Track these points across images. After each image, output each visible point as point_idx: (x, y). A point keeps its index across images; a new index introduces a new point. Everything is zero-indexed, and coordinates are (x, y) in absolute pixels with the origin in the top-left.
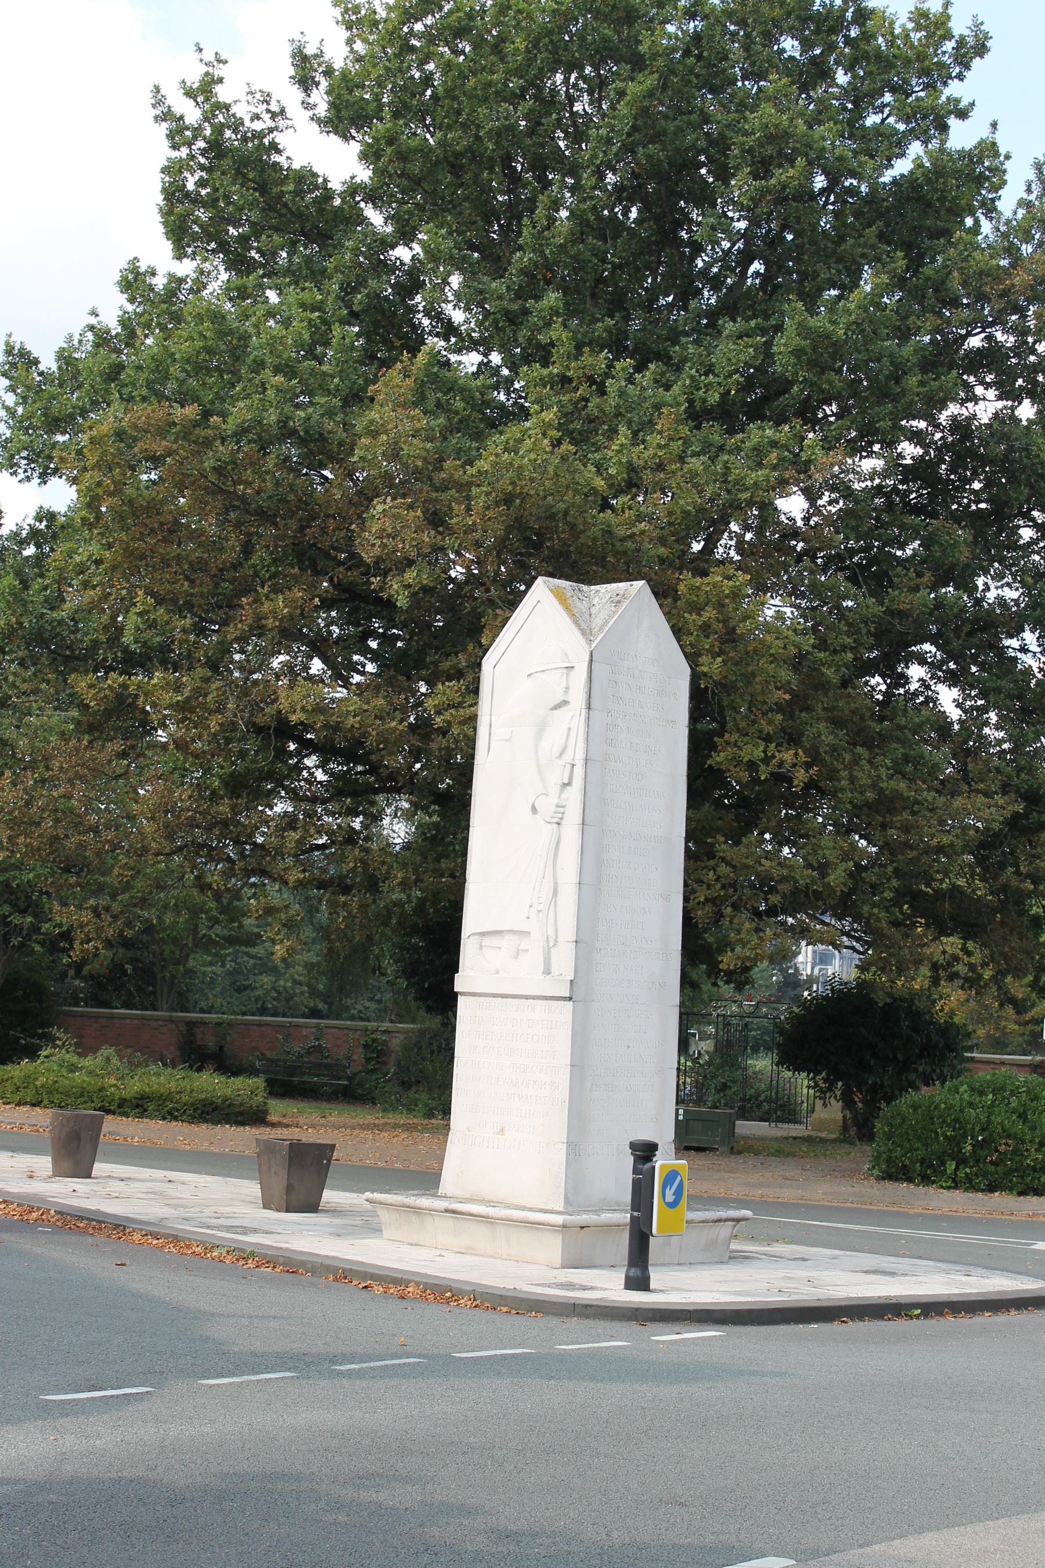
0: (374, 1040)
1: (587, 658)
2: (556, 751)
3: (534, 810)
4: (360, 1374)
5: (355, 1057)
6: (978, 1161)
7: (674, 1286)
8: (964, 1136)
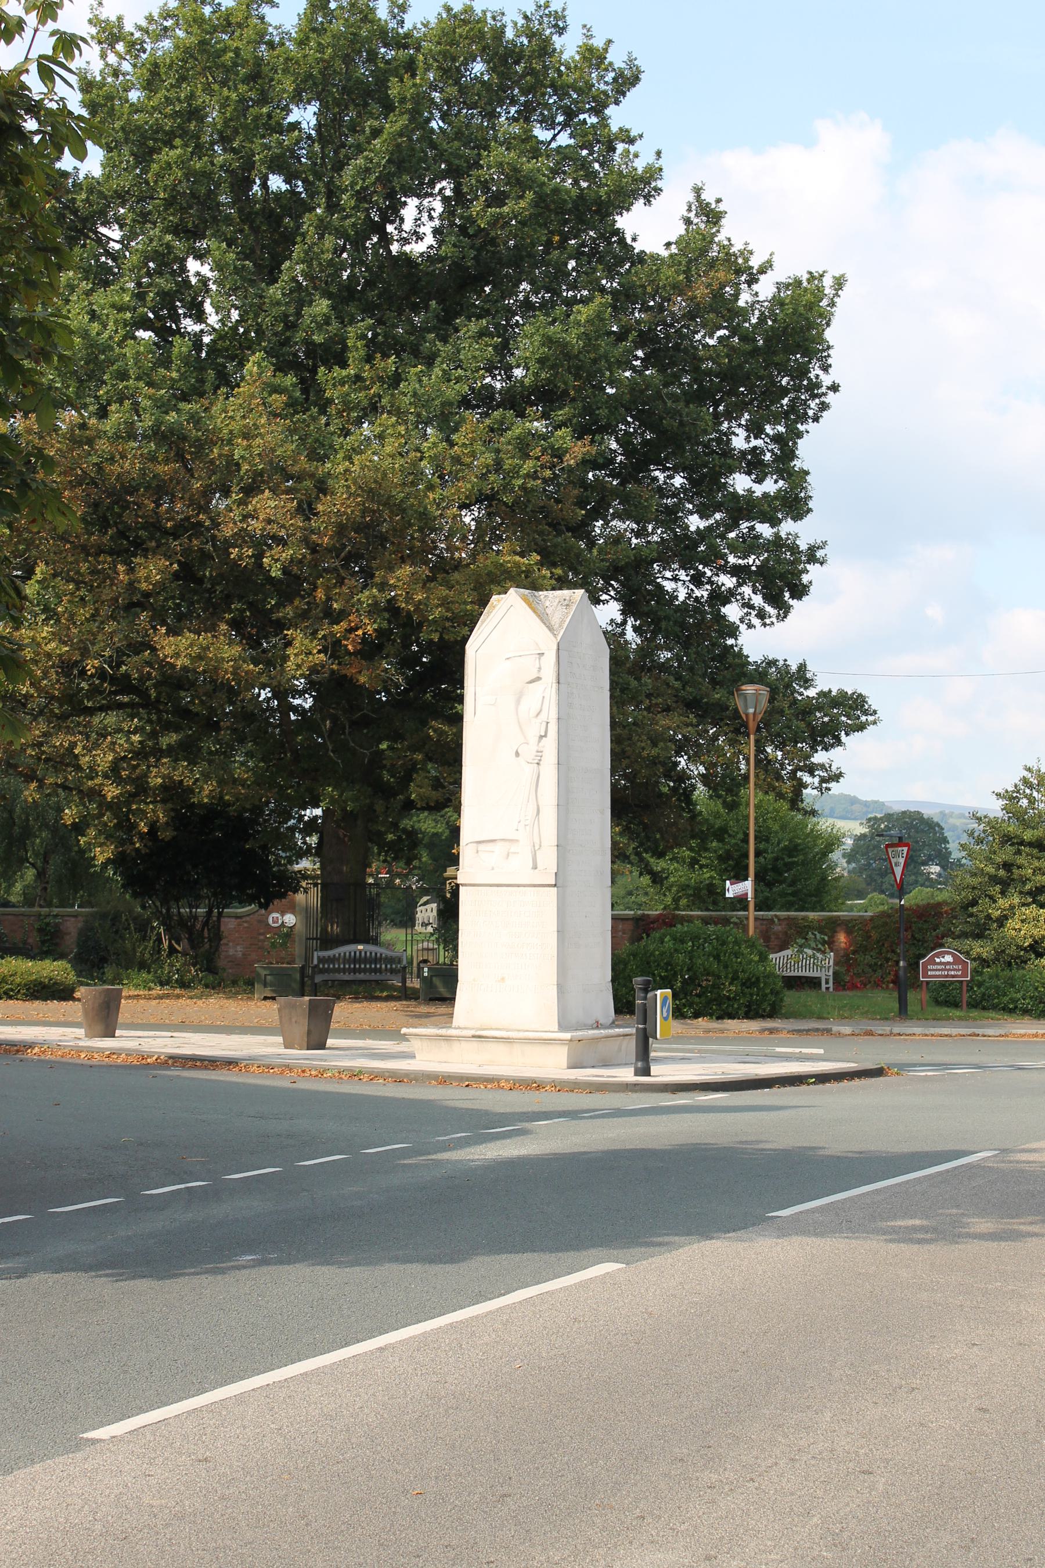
0: (48, 924)
1: (555, 647)
2: (533, 713)
3: (517, 754)
4: (591, 1117)
5: (30, 941)
6: (686, 994)
7: (662, 1073)
8: (675, 974)
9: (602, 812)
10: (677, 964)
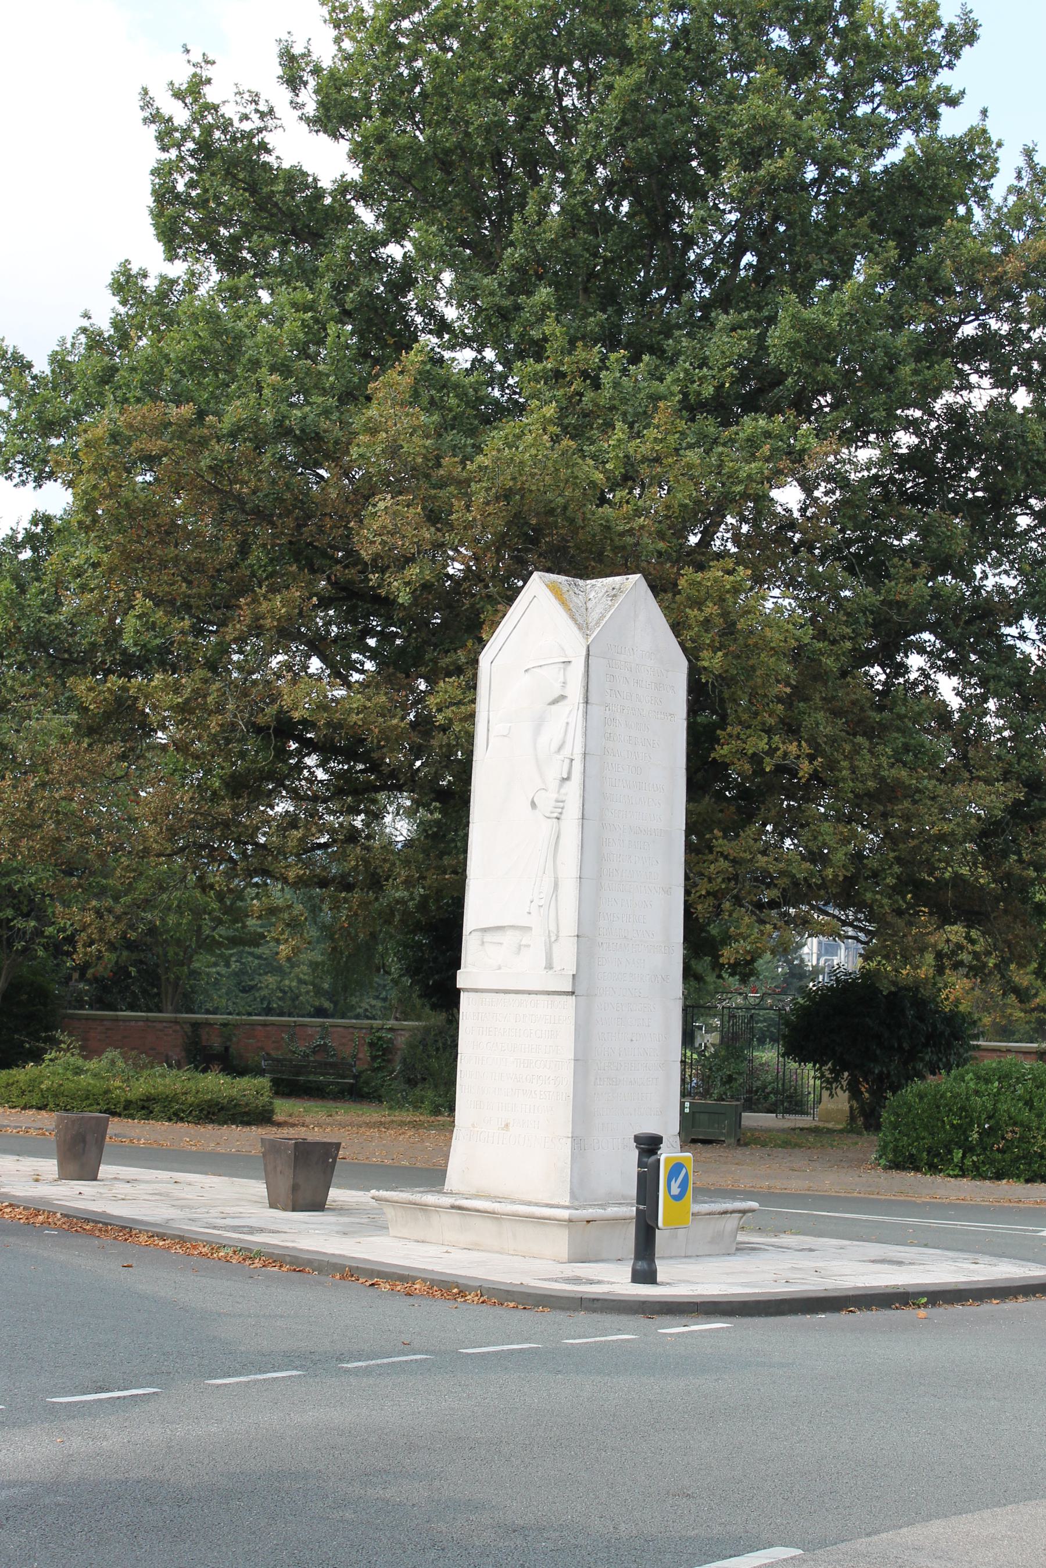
0: (380, 1038)
1: (584, 653)
2: (554, 746)
3: (533, 805)
6: (985, 1149)
7: (680, 1278)
8: (971, 1124)
9: (668, 891)
10: (974, 1110)
